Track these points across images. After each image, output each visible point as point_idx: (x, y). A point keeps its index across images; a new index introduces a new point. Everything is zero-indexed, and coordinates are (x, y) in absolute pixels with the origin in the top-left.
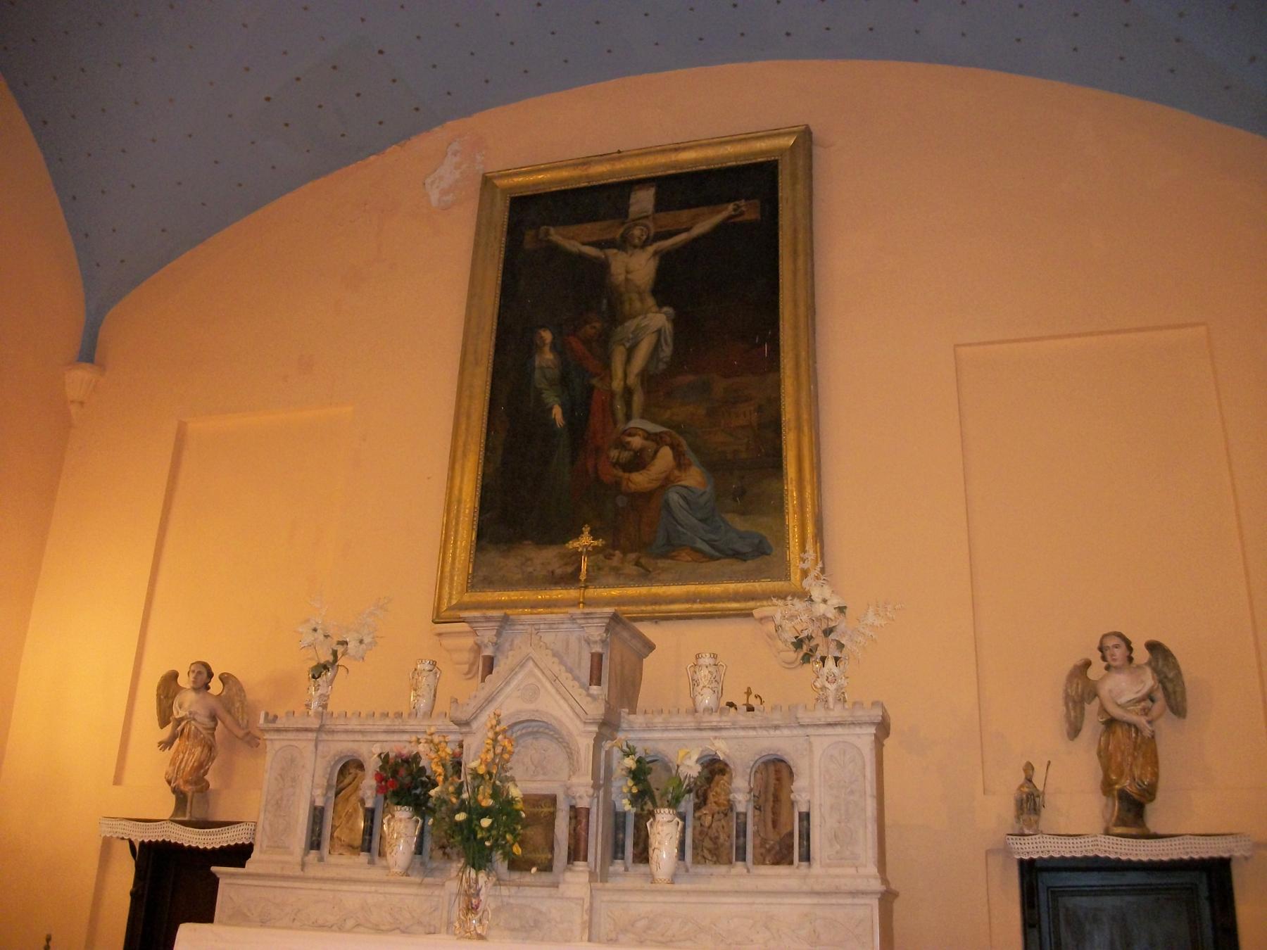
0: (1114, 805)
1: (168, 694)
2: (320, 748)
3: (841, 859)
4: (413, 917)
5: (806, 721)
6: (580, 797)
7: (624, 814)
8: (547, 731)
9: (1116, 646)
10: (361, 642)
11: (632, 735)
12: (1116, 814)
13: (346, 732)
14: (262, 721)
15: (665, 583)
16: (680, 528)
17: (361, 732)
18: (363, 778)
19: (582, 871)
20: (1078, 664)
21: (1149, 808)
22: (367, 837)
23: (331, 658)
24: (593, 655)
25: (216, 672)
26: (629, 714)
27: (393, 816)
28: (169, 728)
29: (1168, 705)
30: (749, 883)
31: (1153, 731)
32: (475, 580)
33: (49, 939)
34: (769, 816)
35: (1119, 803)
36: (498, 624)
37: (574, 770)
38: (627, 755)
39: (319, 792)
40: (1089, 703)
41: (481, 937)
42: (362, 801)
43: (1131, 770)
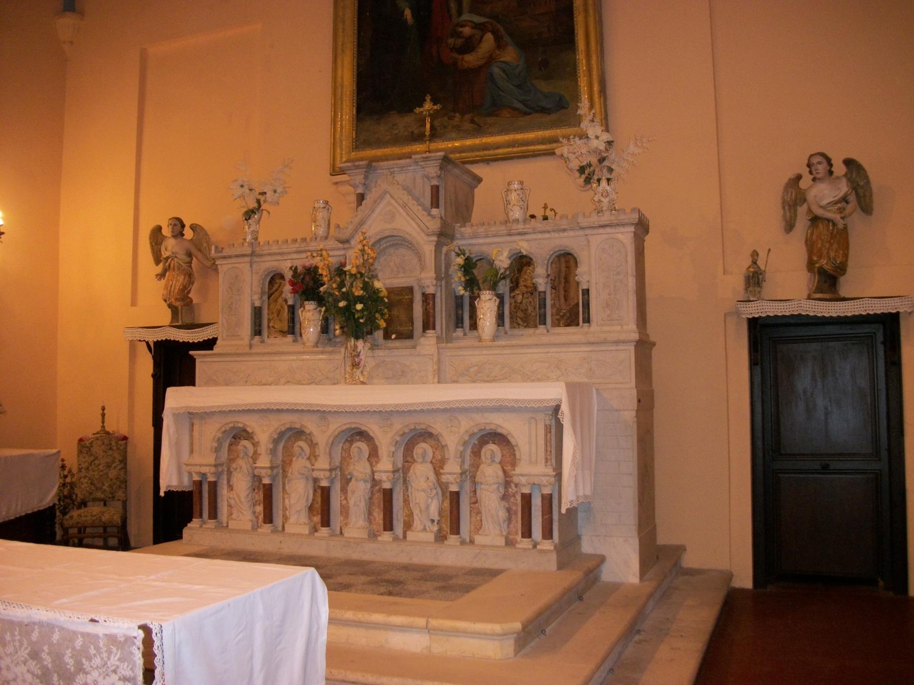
0: (815, 278)
1: (157, 242)
2: (254, 266)
3: (612, 320)
4: (323, 374)
5: (584, 224)
6: (428, 286)
7: (462, 297)
8: (403, 243)
9: (819, 163)
10: (275, 191)
11: (464, 242)
12: (815, 285)
13: (270, 254)
14: (213, 252)
15: (492, 134)
16: (501, 93)
17: (280, 254)
18: (284, 285)
19: (431, 337)
20: (792, 178)
21: (842, 279)
22: (291, 325)
23: (256, 205)
24: (432, 186)
25: (187, 224)
26: (461, 227)
27: (304, 308)
28: (161, 265)
29: (859, 205)
30: (545, 339)
31: (845, 225)
32: (358, 143)
33: (103, 409)
34: (562, 293)
35: (818, 277)
36: (364, 170)
37: (423, 268)
38: (458, 255)
39: (256, 297)
40: (801, 206)
41: (363, 383)
42: (286, 301)
43: (828, 253)
